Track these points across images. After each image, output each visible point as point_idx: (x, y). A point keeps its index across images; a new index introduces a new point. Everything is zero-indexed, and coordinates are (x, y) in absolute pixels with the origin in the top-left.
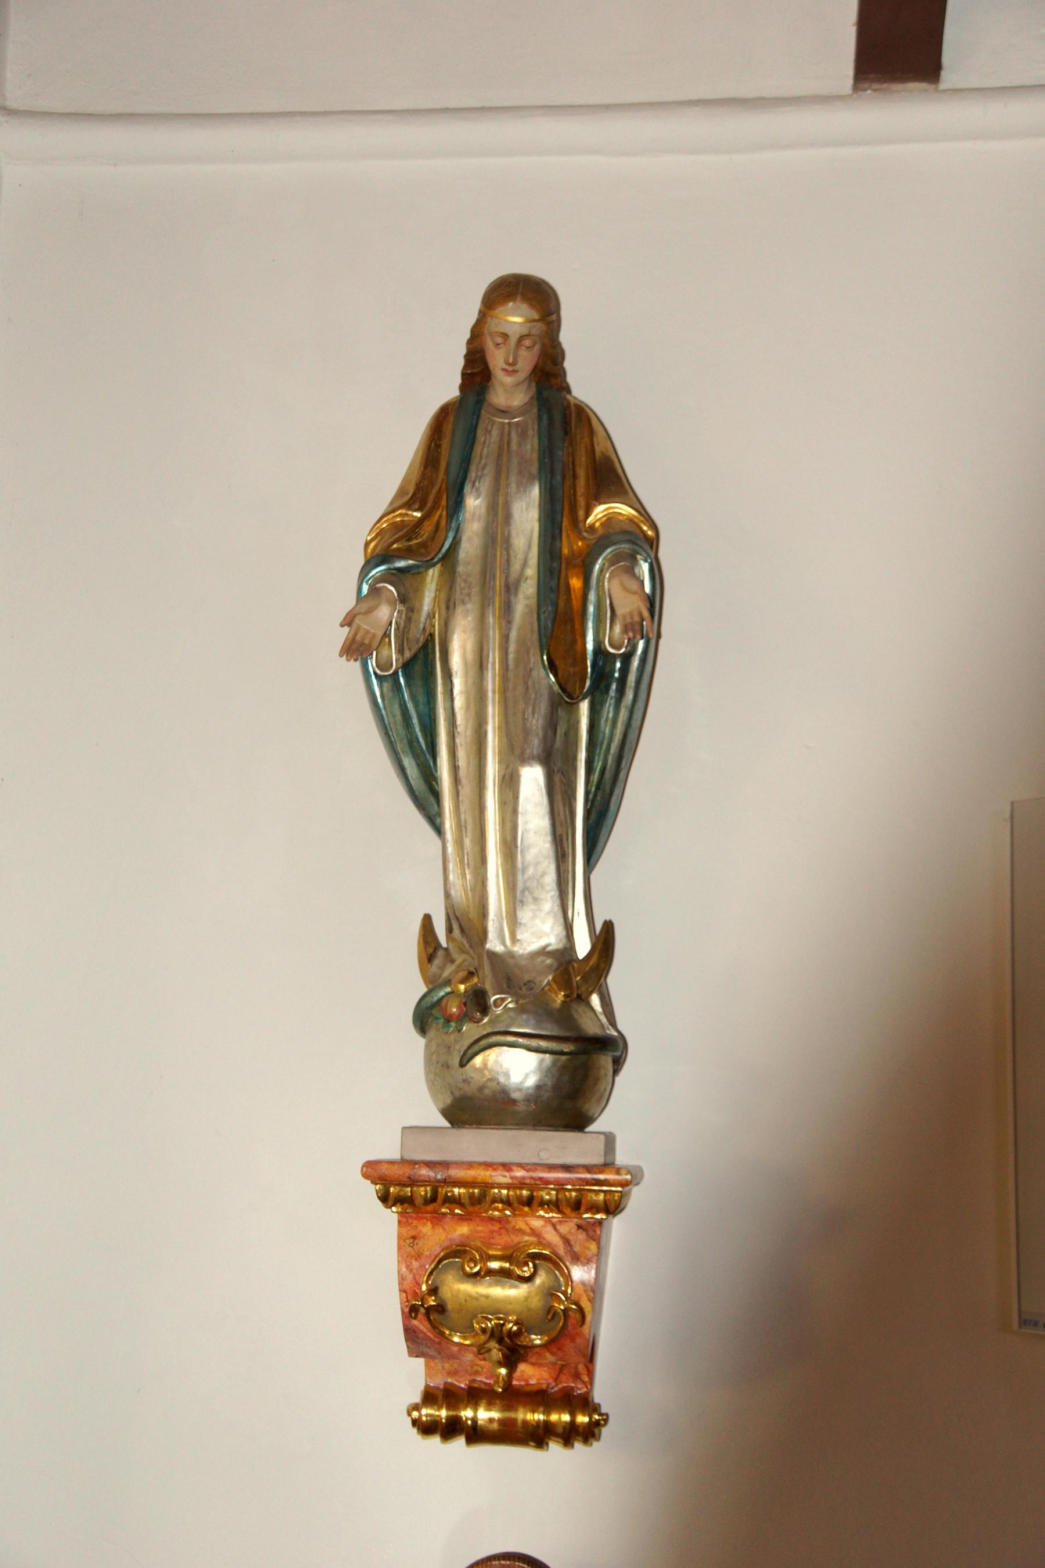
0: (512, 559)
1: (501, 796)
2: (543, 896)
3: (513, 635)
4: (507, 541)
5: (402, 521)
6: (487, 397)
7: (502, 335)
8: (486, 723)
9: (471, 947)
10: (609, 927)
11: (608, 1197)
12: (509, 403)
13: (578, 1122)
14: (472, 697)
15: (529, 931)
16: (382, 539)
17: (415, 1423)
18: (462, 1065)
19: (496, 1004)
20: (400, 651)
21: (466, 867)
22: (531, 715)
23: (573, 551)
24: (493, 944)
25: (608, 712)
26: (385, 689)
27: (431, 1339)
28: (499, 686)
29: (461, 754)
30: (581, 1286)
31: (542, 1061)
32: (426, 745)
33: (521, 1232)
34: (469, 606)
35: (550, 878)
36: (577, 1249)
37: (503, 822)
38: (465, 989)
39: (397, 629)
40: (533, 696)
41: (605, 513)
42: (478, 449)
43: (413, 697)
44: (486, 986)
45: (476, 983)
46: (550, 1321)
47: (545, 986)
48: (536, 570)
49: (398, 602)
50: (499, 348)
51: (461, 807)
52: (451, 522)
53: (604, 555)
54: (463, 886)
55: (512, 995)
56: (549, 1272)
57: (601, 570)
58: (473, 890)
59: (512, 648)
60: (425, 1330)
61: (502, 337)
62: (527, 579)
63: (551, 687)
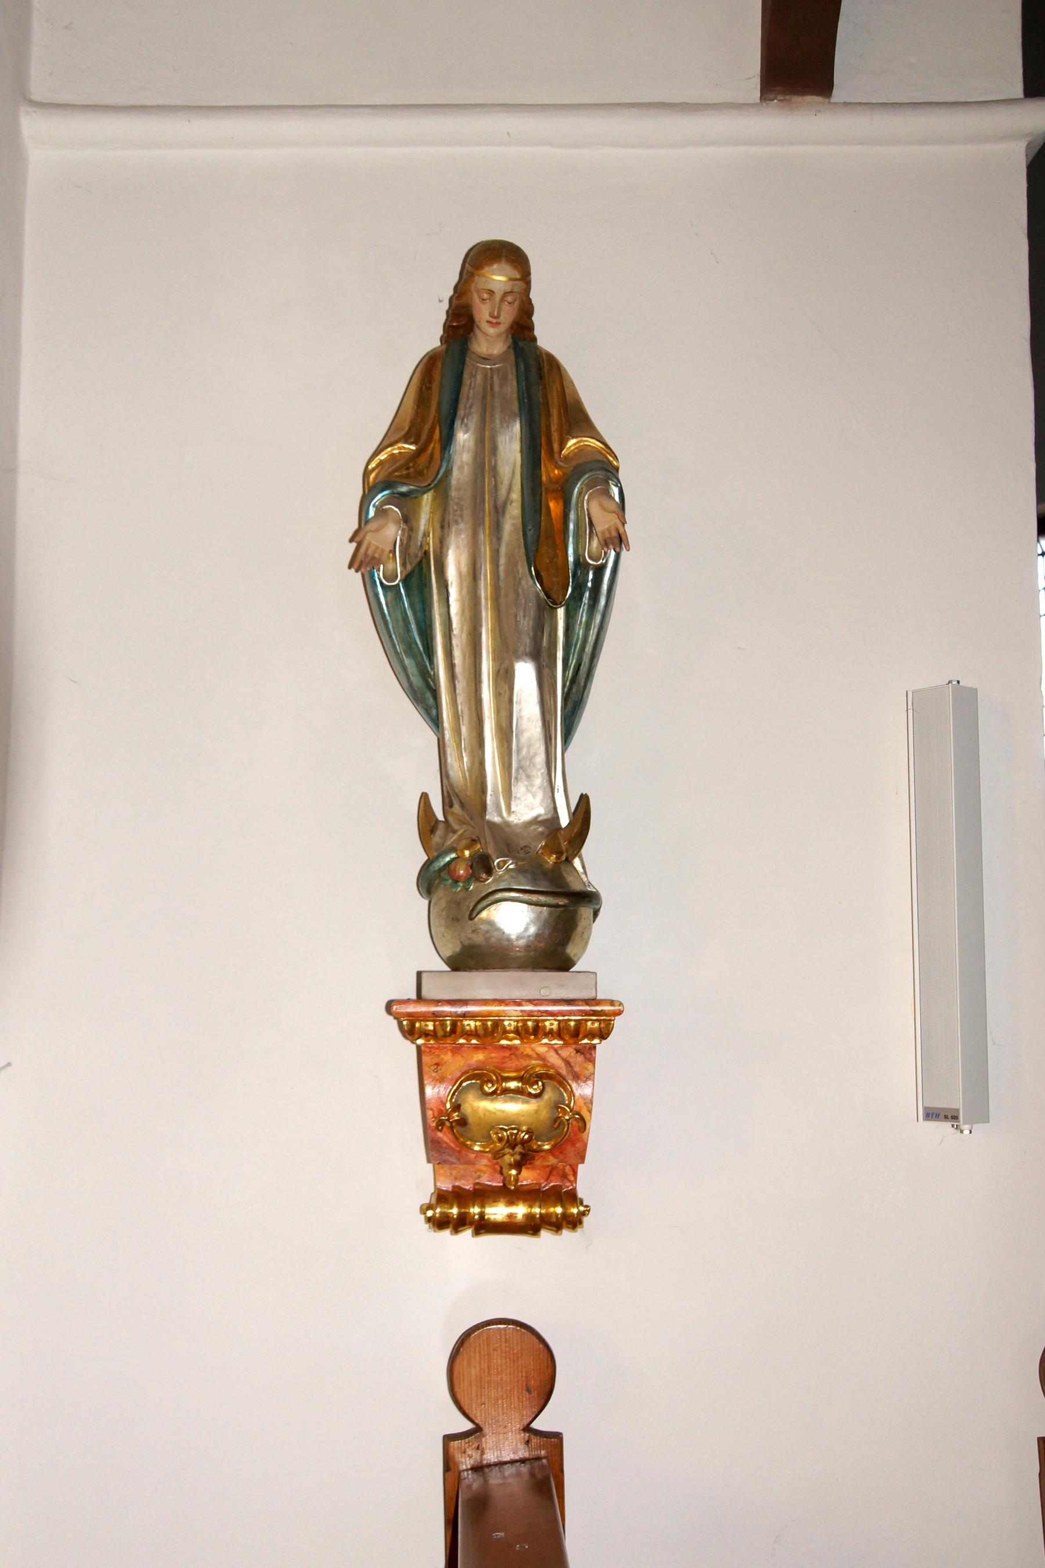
0: (499, 485)
1: (496, 688)
2: (534, 773)
3: (503, 550)
4: (494, 470)
5: (400, 453)
6: (470, 346)
7: (489, 291)
8: (481, 626)
9: (471, 819)
10: (584, 800)
11: (602, 1025)
12: (490, 352)
13: (564, 964)
14: (466, 604)
15: (523, 803)
16: (382, 469)
17: (429, 1220)
18: (471, 919)
19: (500, 867)
20: (404, 564)
21: (463, 751)
22: (522, 618)
23: (550, 478)
24: (492, 816)
25: (582, 616)
26: (389, 598)
27: (452, 1148)
28: (491, 593)
29: (457, 653)
30: (581, 1100)
31: (541, 913)
32: (423, 647)
33: (529, 1056)
34: (462, 526)
35: (540, 758)
36: (577, 1069)
37: (498, 711)
38: (470, 854)
39: (401, 545)
40: (523, 601)
41: (577, 445)
42: (465, 390)
43: (411, 605)
44: (489, 850)
45: (479, 849)
46: (555, 1129)
47: (539, 850)
48: (520, 494)
49: (402, 522)
50: (484, 303)
51: (458, 699)
52: (445, 453)
53: (582, 480)
54: (460, 767)
55: (513, 858)
56: (554, 1088)
57: (580, 493)
58: (470, 770)
59: (502, 561)
60: (448, 1141)
61: (489, 293)
62: (512, 502)
63: (537, 594)
